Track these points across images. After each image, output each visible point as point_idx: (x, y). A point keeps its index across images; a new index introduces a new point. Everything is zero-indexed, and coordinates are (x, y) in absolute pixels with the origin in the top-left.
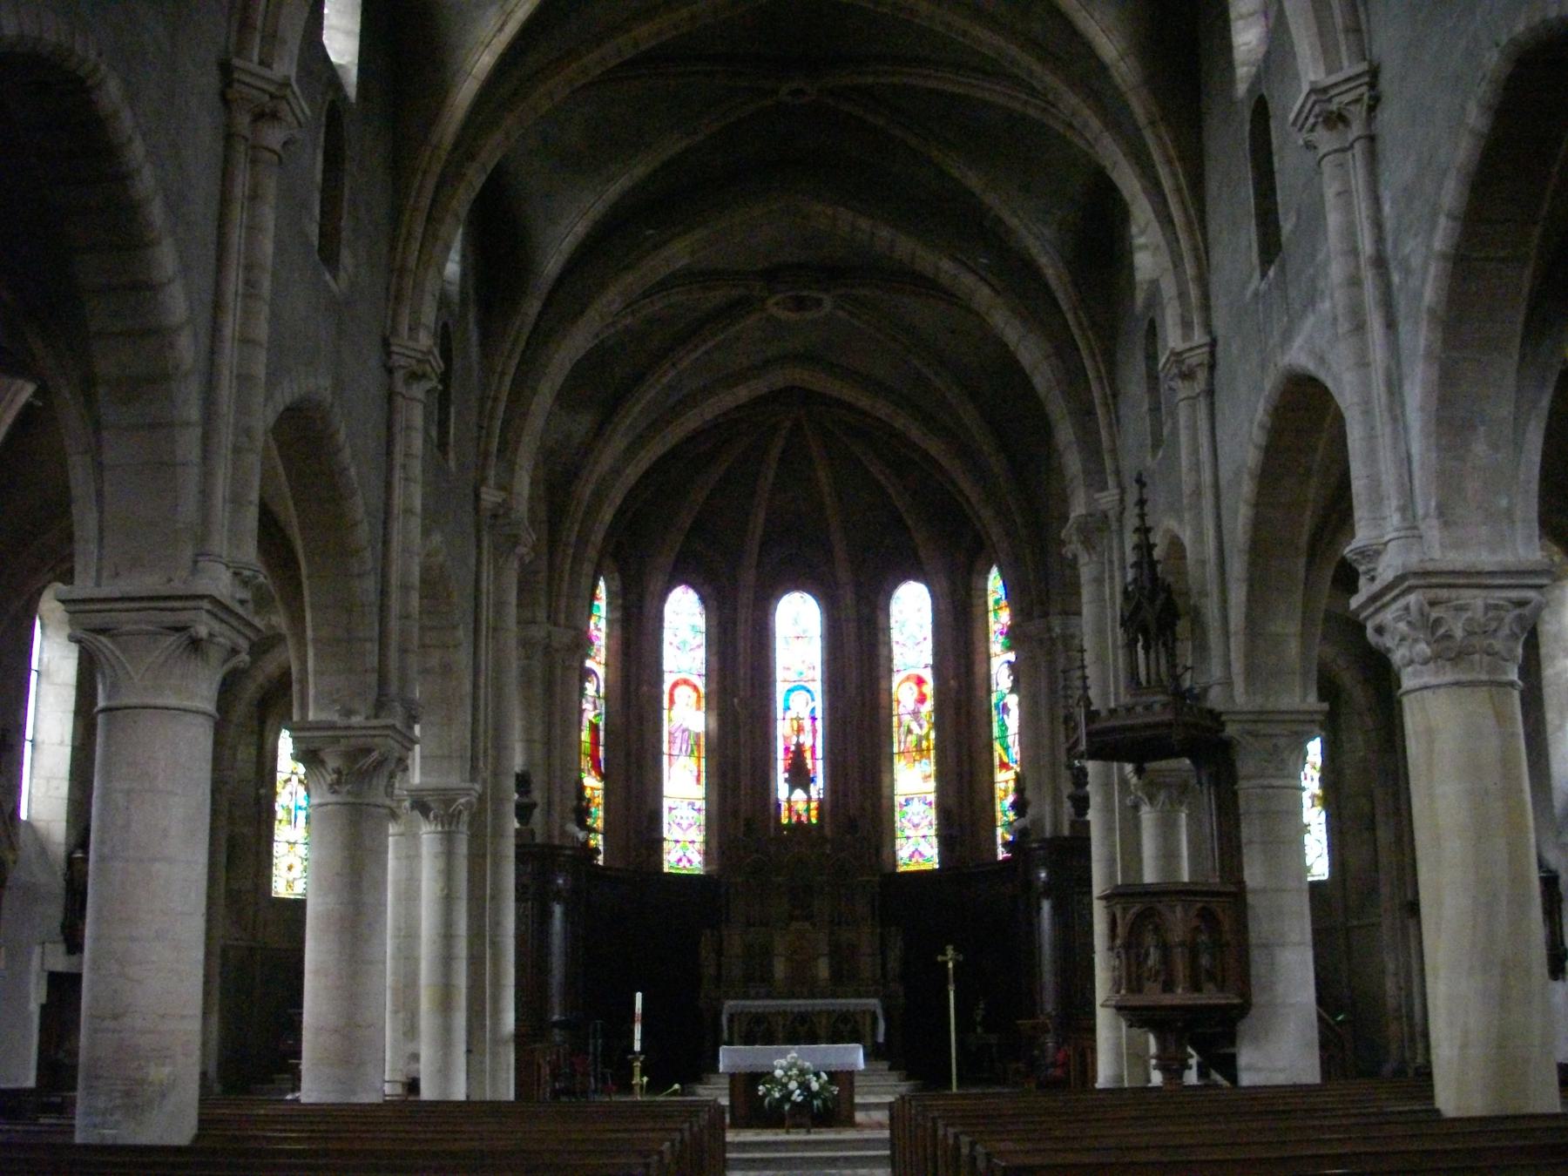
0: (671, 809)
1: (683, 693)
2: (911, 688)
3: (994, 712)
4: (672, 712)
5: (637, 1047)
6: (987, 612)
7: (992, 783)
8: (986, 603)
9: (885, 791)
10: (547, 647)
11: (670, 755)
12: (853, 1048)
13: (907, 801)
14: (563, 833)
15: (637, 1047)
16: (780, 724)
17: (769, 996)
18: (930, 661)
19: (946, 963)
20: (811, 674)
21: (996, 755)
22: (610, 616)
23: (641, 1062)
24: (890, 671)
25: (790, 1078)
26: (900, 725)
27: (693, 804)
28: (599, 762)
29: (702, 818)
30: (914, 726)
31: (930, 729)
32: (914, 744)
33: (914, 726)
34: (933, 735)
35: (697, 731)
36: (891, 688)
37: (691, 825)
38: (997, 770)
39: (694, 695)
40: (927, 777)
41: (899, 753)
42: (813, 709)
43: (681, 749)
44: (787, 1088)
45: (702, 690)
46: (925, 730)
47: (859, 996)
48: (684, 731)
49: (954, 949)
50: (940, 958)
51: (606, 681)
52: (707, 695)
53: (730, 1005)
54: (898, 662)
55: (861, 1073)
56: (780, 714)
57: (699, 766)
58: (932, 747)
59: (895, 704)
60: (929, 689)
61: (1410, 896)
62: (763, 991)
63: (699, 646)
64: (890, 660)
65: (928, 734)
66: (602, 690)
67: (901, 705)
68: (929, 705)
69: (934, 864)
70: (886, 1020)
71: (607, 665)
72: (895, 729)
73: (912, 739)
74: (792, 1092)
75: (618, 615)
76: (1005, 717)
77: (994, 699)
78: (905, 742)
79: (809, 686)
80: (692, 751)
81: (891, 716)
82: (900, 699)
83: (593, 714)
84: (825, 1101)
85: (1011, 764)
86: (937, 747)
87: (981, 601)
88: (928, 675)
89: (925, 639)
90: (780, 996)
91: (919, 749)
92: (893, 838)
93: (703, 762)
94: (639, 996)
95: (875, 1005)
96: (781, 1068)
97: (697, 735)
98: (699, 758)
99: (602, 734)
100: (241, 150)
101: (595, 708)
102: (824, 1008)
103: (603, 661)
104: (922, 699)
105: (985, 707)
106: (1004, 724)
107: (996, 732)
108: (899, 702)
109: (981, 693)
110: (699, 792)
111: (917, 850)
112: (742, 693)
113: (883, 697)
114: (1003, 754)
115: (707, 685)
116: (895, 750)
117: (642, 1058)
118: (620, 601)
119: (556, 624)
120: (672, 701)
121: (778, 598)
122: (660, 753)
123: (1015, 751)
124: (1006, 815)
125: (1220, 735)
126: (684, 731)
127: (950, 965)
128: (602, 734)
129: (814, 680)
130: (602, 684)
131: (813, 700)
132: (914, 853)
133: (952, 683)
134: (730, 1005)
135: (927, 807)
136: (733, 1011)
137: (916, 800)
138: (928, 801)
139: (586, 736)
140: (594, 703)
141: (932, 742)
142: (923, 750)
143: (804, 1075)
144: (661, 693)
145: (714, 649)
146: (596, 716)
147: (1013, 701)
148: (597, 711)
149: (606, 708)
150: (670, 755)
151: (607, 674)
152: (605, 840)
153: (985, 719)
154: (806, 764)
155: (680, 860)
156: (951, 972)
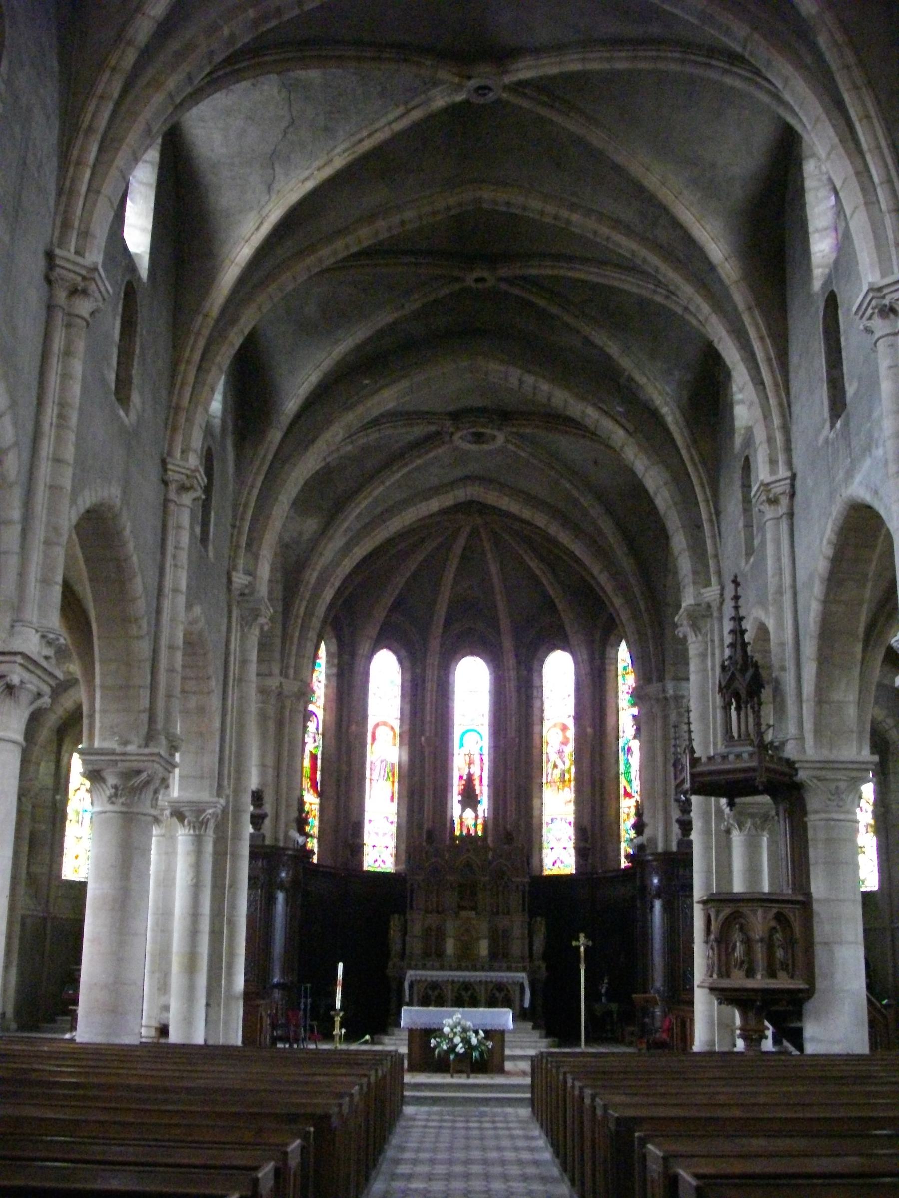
3: (621, 754)
5: (338, 1005)
13: (552, 820)
14: (287, 837)
15: (338, 1005)
17: (442, 968)
19: (579, 948)
25: (455, 1034)
30: (559, 763)
33: (559, 763)
39: (391, 733)
45: (397, 731)
47: (509, 969)
49: (586, 937)
53: (410, 975)
55: (510, 1032)
65: (570, 769)
71: (325, 709)
72: (544, 764)
73: (557, 772)
74: (457, 1045)
75: (334, 670)
80: (388, 777)
84: (482, 1054)
87: (613, 668)
88: (571, 723)
90: (451, 969)
91: (562, 779)
93: (396, 785)
94: (340, 966)
96: (449, 1026)
97: (393, 765)
102: (484, 979)
103: (322, 706)
107: (622, 769)
109: (611, 738)
113: (536, 737)
116: (544, 781)
117: (341, 1014)
118: (336, 661)
119: (286, 676)
127: (582, 949)
134: (410, 975)
141: (573, 775)
145: (407, 699)
147: (635, 745)
151: (324, 715)
153: (613, 761)
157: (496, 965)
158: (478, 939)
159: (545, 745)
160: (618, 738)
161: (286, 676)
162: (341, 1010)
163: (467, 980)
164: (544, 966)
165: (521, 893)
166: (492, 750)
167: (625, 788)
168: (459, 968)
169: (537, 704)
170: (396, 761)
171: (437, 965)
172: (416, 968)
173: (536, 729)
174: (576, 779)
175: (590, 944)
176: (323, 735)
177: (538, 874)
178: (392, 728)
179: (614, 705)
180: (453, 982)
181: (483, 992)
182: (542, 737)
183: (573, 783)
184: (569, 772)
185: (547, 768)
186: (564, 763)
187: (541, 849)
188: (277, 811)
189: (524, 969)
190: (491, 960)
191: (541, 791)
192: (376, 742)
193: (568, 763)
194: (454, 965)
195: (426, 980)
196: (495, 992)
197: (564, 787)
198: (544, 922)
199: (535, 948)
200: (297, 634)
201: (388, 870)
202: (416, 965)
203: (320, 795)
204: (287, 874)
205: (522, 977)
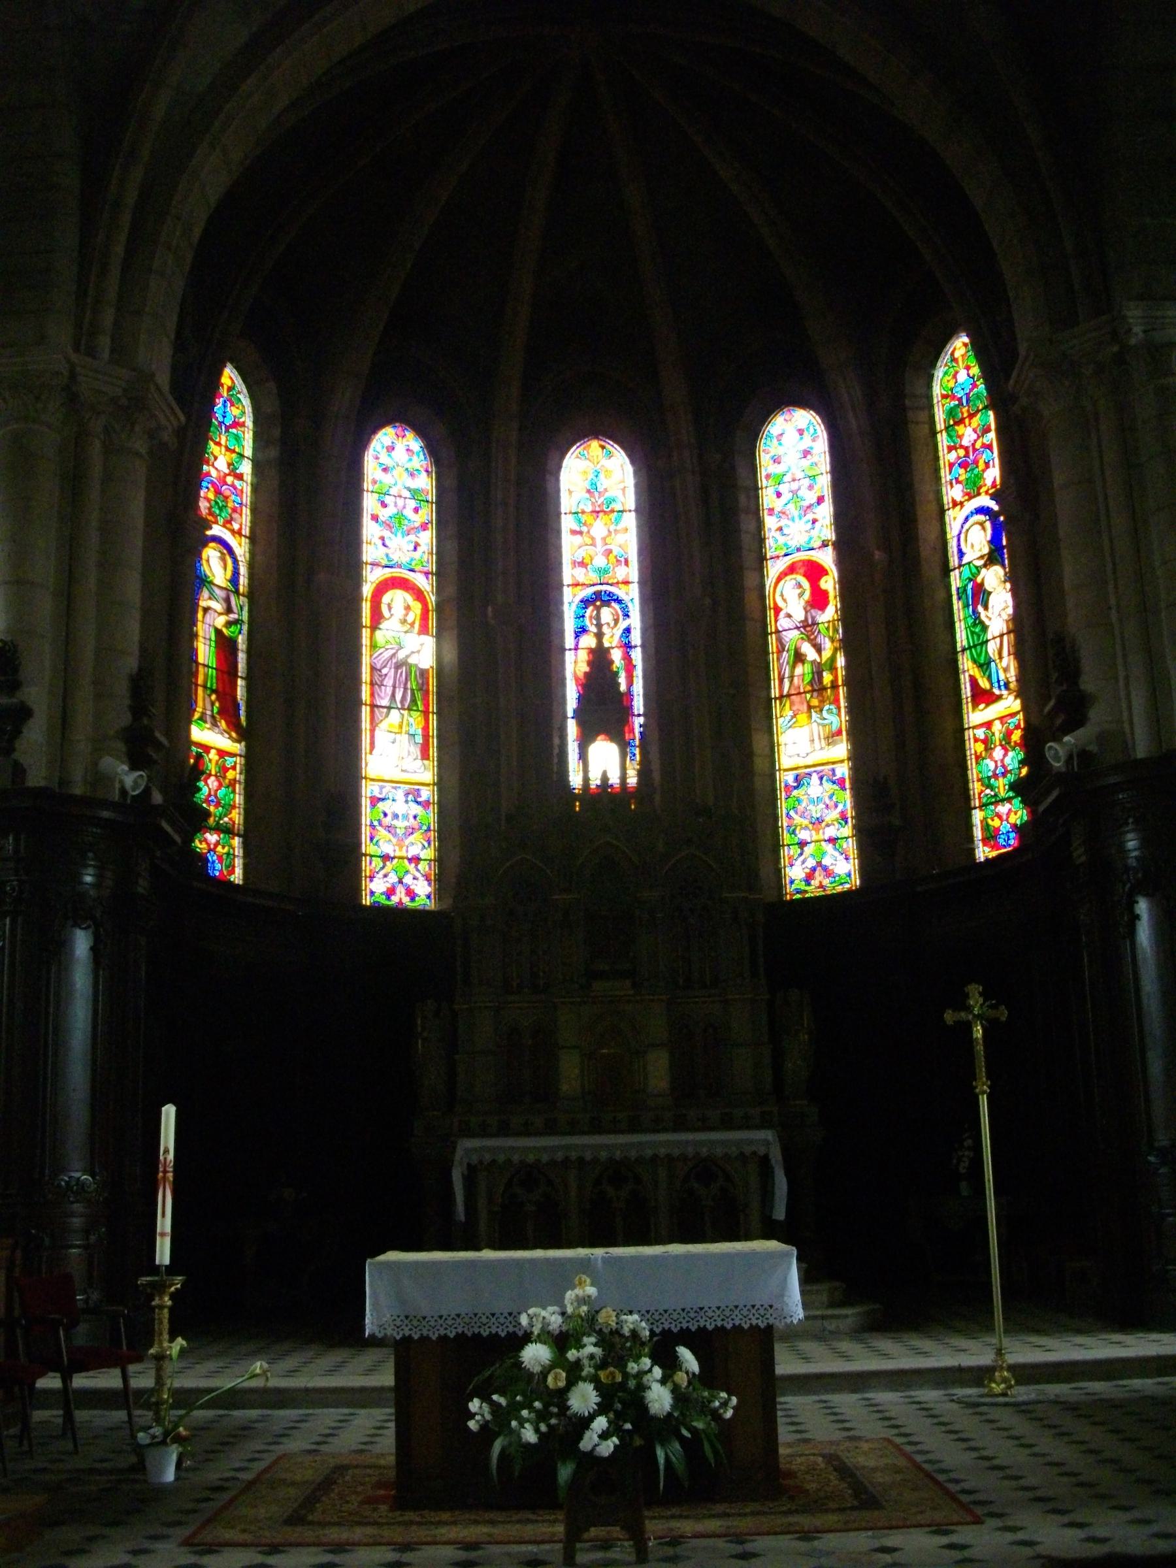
0: (375, 801)
1: (396, 599)
2: (799, 586)
3: (957, 605)
4: (378, 633)
5: (163, 1253)
6: (933, 433)
7: (960, 730)
8: (932, 418)
9: (759, 764)
10: (72, 399)
11: (373, 706)
12: (770, 1255)
13: (797, 779)
14: (99, 779)
15: (163, 1253)
16: (569, 657)
17: (550, 1129)
18: (830, 534)
19: (967, 1027)
20: (621, 573)
21: (965, 680)
22: (260, 455)
23: (173, 1296)
24: (762, 559)
25: (574, 1372)
26: (781, 648)
27: (417, 793)
28: (237, 706)
29: (430, 817)
30: (808, 650)
31: (836, 650)
32: (808, 678)
33: (808, 650)
34: (841, 661)
36: (762, 586)
37: (411, 831)
38: (967, 707)
39: (417, 607)
40: (832, 737)
41: (781, 697)
42: (628, 630)
43: (393, 695)
44: (564, 1408)
45: (432, 599)
46: (827, 654)
47: (727, 1123)
48: (398, 666)
49: (985, 995)
50: (949, 1017)
51: (251, 566)
52: (439, 607)
53: (468, 1148)
54: (774, 543)
55: (793, 1334)
56: (569, 641)
57: (426, 729)
58: (840, 682)
59: (771, 614)
60: (829, 583)
63: (424, 527)
64: (761, 541)
65: (833, 659)
66: (243, 581)
67: (782, 614)
68: (830, 613)
69: (856, 881)
70: (788, 1173)
71: (252, 539)
72: (773, 658)
74: (585, 1423)
75: (273, 453)
76: (980, 609)
77: (956, 581)
78: (792, 677)
79: (619, 592)
80: (414, 701)
81: (765, 634)
82: (780, 603)
83: (220, 621)
84: (692, 1447)
85: (996, 691)
87: (923, 416)
88: (827, 558)
90: (574, 1129)
91: (817, 686)
92: (776, 846)
93: (433, 720)
94: (169, 1112)
95: (767, 1143)
96: (547, 1337)
97: (423, 673)
98: (426, 713)
99: (242, 657)
101: (229, 610)
103: (246, 531)
104: (819, 600)
105: (941, 595)
106: (977, 620)
107: (962, 637)
108: (777, 610)
109: (930, 571)
110: (425, 773)
111: (819, 864)
112: (500, 598)
113: (751, 598)
114: (976, 673)
115: (439, 590)
116: (774, 692)
117: (177, 1283)
118: (277, 432)
119: (92, 352)
120: (377, 617)
121: (589, 746)
122: (356, 703)
123: (1007, 668)
124: (991, 787)
126: (398, 666)
127: (978, 1032)
128: (242, 657)
129: (626, 583)
130: (243, 570)
131: (627, 615)
132: (814, 870)
133: (878, 555)
134: (468, 1148)
135: (836, 787)
136: (475, 1159)
137: (815, 777)
138: (839, 775)
139: (205, 652)
140: (227, 600)
141: (841, 673)
142: (825, 689)
143: (621, 1364)
144: (357, 599)
146: (229, 624)
147: (994, 578)
148: (233, 616)
149: (250, 611)
150: (373, 706)
151: (252, 553)
152: (246, 846)
153: (940, 619)
154: (619, 684)
155: (390, 893)
156: (980, 1048)
160: (946, 571)
161: (92, 352)
162: (172, 1269)
163: (618, 1154)
167: (973, 681)
168: (597, 1128)
172: (484, 1132)
174: (847, 682)
175: (1003, 1014)
176: (251, 595)
179: (931, 496)
182: (762, 597)
183: (842, 692)
184: (833, 669)
185: (778, 664)
188: (64, 712)
189: (764, 1124)
195: (509, 1161)
197: (822, 702)
200: (119, 250)
201: (780, 1437)
203: (243, 734)
204: (99, 876)
205: (764, 1139)
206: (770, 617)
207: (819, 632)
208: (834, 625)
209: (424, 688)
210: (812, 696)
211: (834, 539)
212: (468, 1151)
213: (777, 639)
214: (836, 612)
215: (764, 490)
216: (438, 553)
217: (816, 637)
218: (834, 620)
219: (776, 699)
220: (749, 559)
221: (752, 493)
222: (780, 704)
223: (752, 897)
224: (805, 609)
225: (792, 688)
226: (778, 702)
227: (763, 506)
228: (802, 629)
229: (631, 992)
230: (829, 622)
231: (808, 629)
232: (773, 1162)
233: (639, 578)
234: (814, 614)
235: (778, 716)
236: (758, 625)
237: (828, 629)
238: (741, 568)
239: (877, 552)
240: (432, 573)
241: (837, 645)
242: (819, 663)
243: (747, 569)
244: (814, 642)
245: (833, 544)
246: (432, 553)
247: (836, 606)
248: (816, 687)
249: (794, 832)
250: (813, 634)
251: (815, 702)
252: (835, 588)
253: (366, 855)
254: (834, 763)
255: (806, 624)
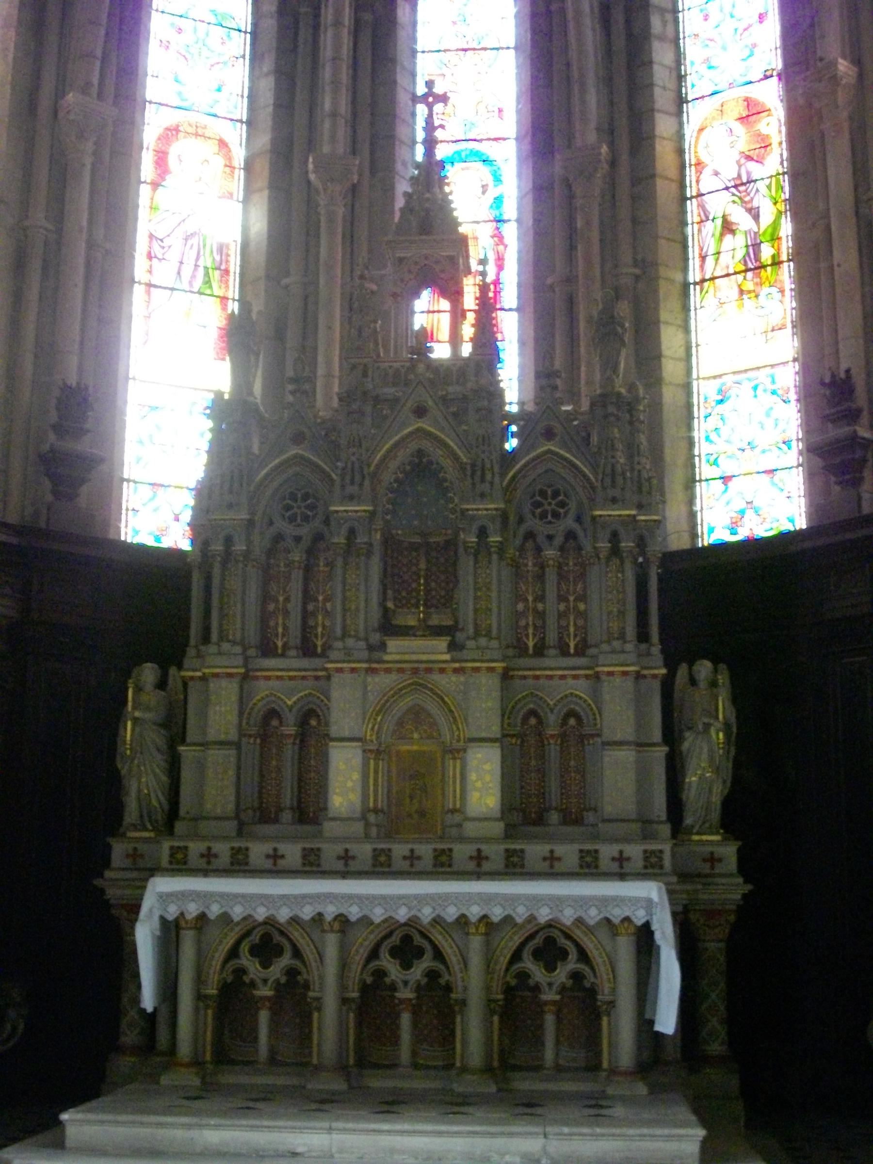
32: (741, 253)
34: (786, 228)
35: (224, 240)
36: (680, 136)
39: (220, 161)
42: (498, 200)
45: (239, 155)
58: (784, 257)
61: (326, 866)
62: (425, 850)
65: (775, 225)
73: (736, 245)
80: (208, 282)
82: (704, 158)
86: (796, 256)
89: (762, 18)
100: (200, 131)
102: (474, 912)
112: (326, 149)
116: (694, 275)
125: (740, 843)
132: (742, 513)
136: (172, 912)
141: (786, 246)
145: (268, 65)
157: (535, 851)
158: (456, 752)
159: (690, 174)
164: (730, 852)
165: (630, 574)
166: (529, 199)
169: (661, 54)
170: (233, 237)
171: (292, 853)
173: (663, 125)
177: (684, 544)
178: (223, 144)
180: (343, 922)
181: (476, 960)
184: (775, 238)
186: (755, 214)
187: (691, 482)
190: (510, 833)
191: (686, 308)
192: (169, 180)
193: (768, 214)
194: (495, 851)
196: (529, 964)
198: (723, 679)
199: (692, 779)
202: (209, 855)
206: (690, 176)
207: (757, 190)
208: (778, 181)
209: (223, 267)
210: (745, 278)
211: (780, 66)
212: (165, 898)
213: (699, 205)
214: (782, 163)
215: (686, 12)
216: (250, 97)
217: (752, 199)
218: (778, 174)
219: (695, 284)
220: (662, 98)
221: (669, 17)
222: (702, 290)
223: (643, 518)
224: (738, 162)
225: (718, 268)
226: (698, 287)
227: (684, 33)
228: (733, 190)
229: (447, 657)
230: (771, 177)
231: (742, 188)
232: (657, 936)
233: (518, 131)
234: (750, 169)
235: (698, 306)
236: (674, 187)
237: (769, 187)
238: (653, 110)
239: (840, 60)
240: (241, 121)
241: (781, 207)
242: (755, 233)
243: (659, 111)
244: (749, 206)
245: (779, 76)
246: (242, 96)
247: (781, 155)
248: (750, 266)
249: (715, 463)
250: (749, 194)
251: (749, 286)
252: (780, 132)
253: (128, 481)
254: (772, 366)
255: (738, 182)
